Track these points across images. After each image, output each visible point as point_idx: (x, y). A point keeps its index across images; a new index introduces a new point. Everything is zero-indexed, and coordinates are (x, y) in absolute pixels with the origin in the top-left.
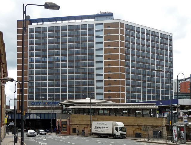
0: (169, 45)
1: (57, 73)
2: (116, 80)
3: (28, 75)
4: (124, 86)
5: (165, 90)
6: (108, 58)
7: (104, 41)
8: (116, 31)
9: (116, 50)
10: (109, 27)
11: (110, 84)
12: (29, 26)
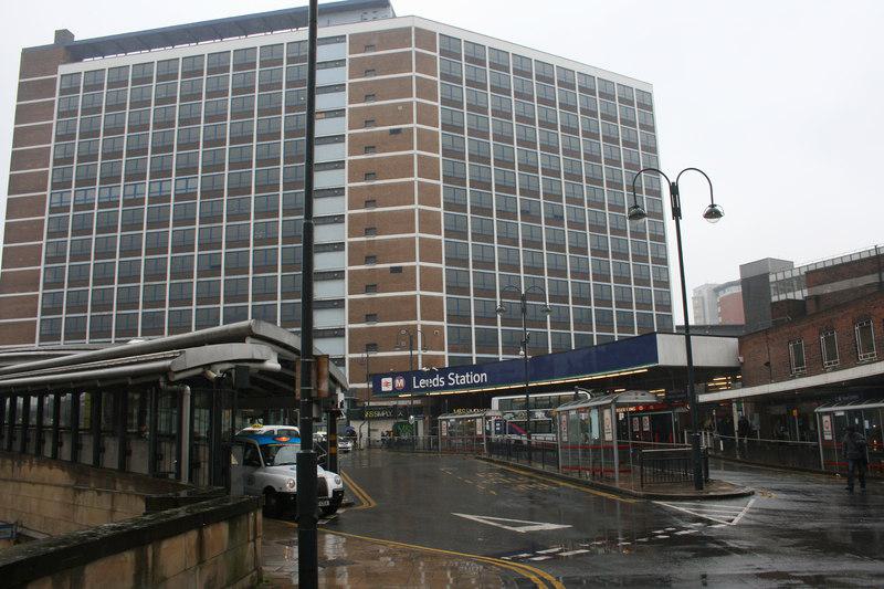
0: (643, 127)
1: (157, 247)
2: (401, 267)
3: (41, 288)
4: (436, 129)
5: (614, 309)
6: (367, 286)
7: (350, 212)
8: (401, 62)
9: (400, 277)
10: (368, 47)
11: (374, 257)
12: (64, 69)
